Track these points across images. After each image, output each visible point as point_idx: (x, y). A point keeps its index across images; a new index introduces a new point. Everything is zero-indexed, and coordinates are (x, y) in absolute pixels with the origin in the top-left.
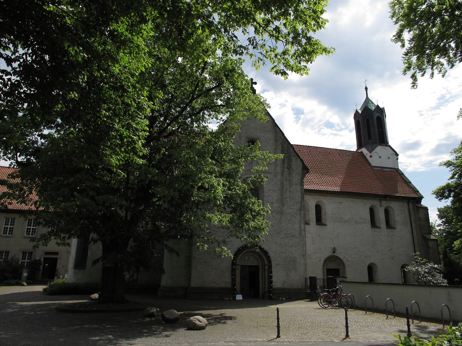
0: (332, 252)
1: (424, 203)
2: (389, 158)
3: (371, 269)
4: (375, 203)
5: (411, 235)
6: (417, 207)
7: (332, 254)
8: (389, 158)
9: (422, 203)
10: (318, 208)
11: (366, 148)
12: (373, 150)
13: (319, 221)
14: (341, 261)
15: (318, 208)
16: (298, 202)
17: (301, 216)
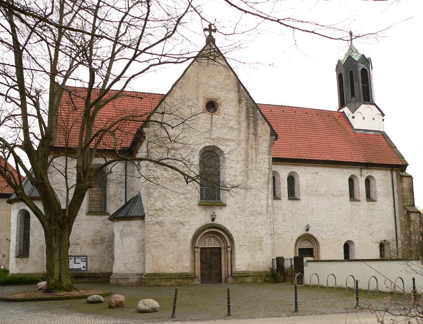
0: (305, 230)
1: (409, 171)
2: (374, 119)
3: (347, 247)
4: (355, 172)
5: (393, 208)
6: (401, 176)
7: (305, 232)
8: (374, 119)
9: (406, 171)
10: (291, 180)
11: (348, 108)
12: (356, 110)
13: (292, 195)
14: (315, 239)
15: (291, 180)
16: (265, 174)
17: (268, 191)
